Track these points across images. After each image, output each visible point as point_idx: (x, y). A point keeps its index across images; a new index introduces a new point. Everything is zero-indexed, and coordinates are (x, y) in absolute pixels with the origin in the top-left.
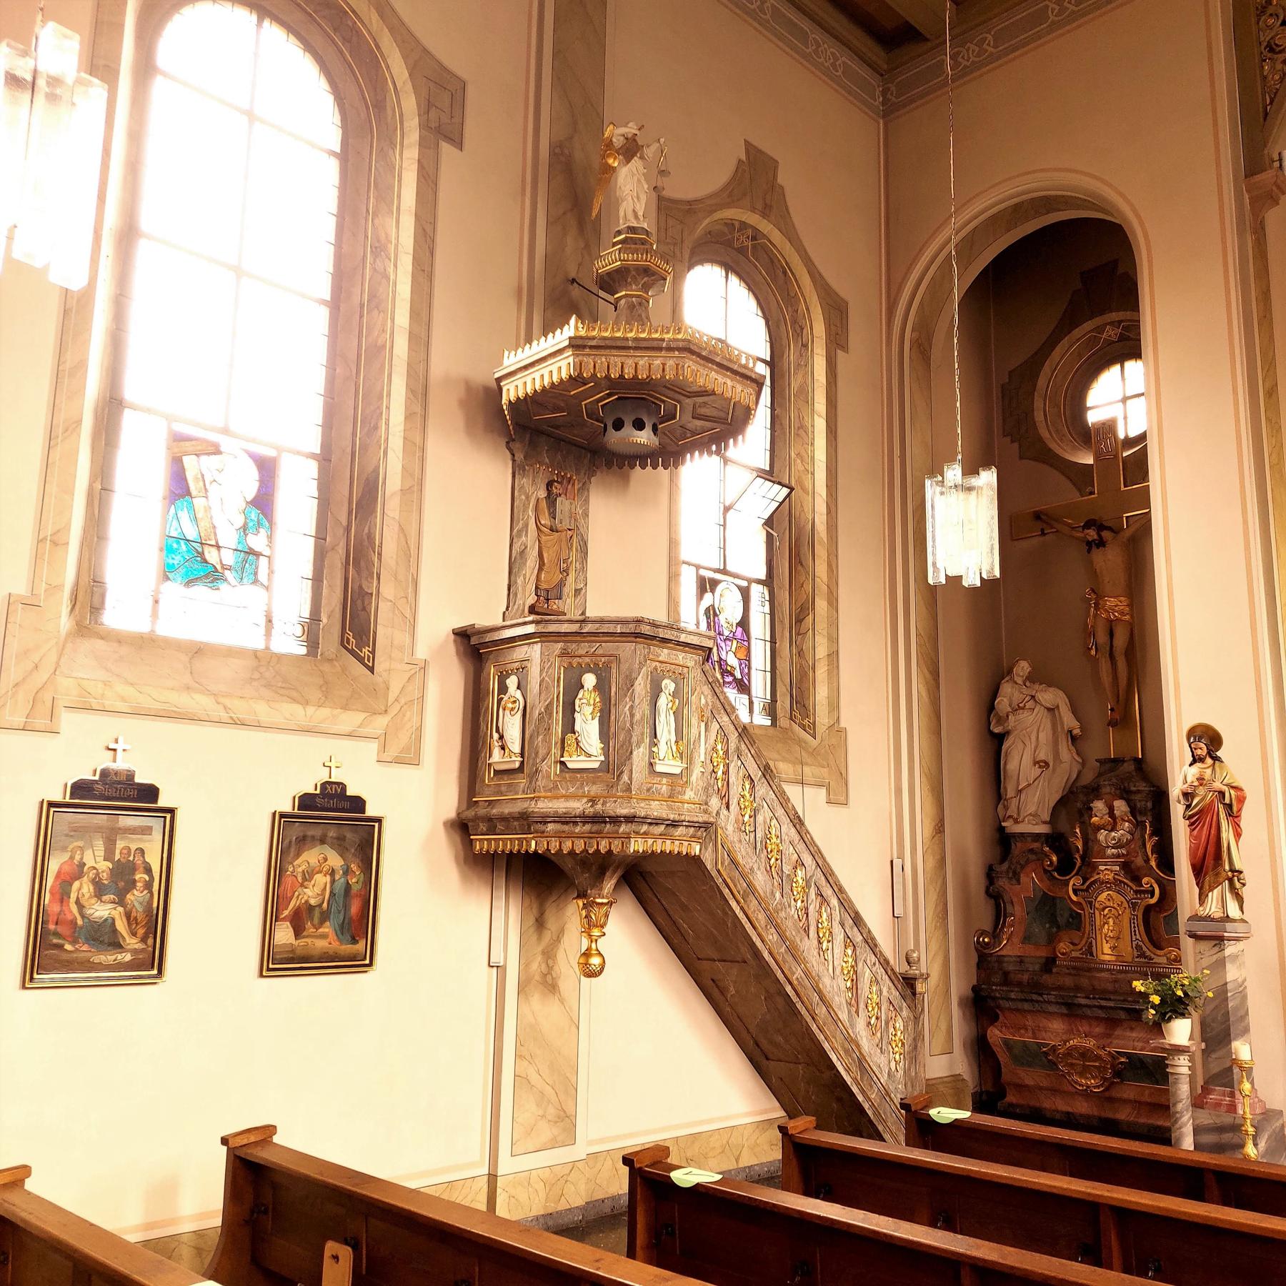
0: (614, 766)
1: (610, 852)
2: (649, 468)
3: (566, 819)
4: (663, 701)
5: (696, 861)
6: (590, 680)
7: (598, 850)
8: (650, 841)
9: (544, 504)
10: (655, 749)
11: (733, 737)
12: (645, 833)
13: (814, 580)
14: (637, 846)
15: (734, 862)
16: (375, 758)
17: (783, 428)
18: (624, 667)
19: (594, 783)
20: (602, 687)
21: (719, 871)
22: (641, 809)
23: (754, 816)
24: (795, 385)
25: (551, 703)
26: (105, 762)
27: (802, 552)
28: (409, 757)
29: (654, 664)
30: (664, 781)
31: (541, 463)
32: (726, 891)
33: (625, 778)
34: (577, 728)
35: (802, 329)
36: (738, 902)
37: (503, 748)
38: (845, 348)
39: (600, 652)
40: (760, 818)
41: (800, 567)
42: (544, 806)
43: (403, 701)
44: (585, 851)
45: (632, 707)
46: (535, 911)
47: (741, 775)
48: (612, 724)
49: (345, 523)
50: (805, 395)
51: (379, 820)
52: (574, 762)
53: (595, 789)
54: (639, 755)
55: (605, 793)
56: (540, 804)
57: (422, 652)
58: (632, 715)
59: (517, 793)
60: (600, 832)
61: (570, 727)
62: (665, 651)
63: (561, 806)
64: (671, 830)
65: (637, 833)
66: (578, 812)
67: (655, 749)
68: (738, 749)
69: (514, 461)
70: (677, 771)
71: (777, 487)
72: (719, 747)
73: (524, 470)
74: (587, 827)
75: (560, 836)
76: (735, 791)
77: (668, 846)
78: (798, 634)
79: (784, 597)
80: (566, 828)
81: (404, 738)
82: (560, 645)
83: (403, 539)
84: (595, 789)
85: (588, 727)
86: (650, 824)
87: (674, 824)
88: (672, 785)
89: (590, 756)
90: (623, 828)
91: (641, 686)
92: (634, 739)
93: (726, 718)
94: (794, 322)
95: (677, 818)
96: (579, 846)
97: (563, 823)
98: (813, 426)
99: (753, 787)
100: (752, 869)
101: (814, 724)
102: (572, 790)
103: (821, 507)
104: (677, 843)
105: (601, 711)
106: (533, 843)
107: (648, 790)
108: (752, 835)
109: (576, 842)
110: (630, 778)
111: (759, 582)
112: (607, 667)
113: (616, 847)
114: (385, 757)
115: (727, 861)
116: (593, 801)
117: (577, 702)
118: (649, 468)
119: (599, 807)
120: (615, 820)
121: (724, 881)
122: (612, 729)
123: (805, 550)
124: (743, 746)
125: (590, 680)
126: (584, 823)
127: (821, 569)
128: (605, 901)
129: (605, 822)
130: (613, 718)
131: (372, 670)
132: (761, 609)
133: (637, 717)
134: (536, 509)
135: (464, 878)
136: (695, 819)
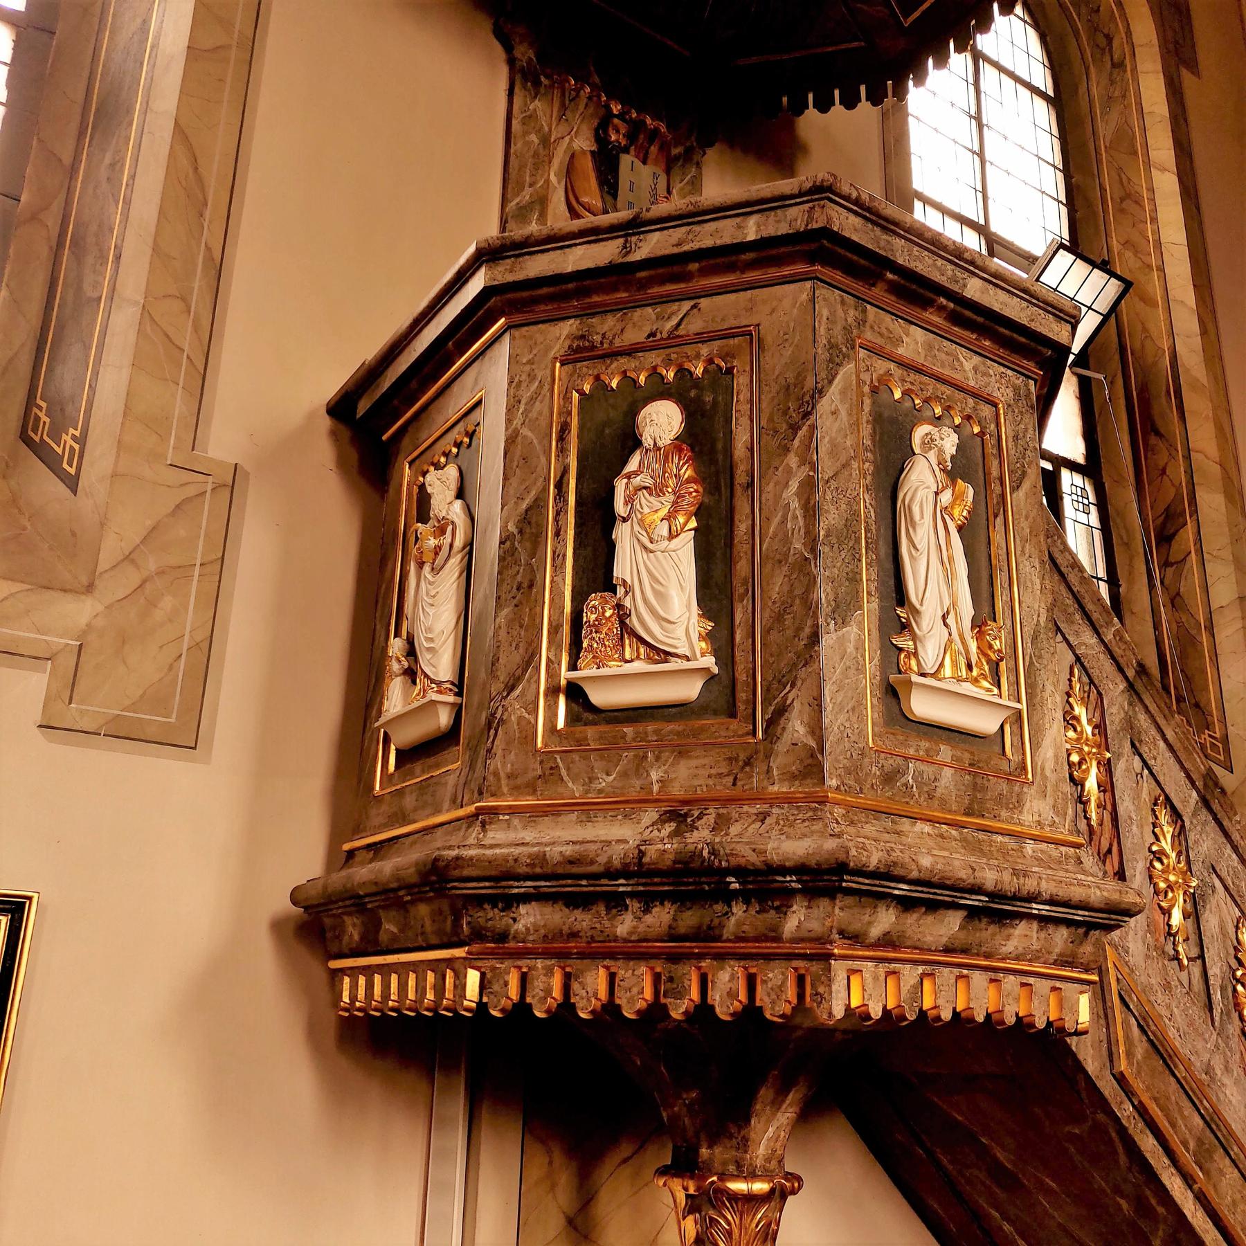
0: (751, 693)
1: (751, 1012)
2: (838, 109)
3: (576, 884)
4: (921, 479)
5: (1047, 1047)
6: (662, 421)
7: (704, 1009)
8: (910, 974)
9: (588, 164)
10: (906, 643)
11: (1115, 690)
12: (888, 942)
13: (1188, 458)
14: (857, 991)
15: (1161, 1051)
16: (38, 717)
17: (1089, 205)
18: (777, 362)
19: (682, 752)
20: (703, 439)
21: (1121, 1079)
22: (869, 845)
23: (1194, 914)
24: (1106, 130)
25: (538, 505)
27: (1156, 412)
28: (171, 724)
29: (882, 366)
30: (945, 752)
31: (582, 79)
32: (1148, 1144)
33: (796, 727)
34: (622, 569)
35: (1109, 39)
36: (1188, 1179)
37: (411, 674)
38: (1193, 66)
39: (695, 325)
40: (1210, 922)
41: (1153, 440)
42: (508, 841)
43: (152, 565)
44: (656, 1011)
45: (809, 486)
46: (564, 1197)
47: (1145, 795)
48: (741, 548)
49: (67, 159)
50: (1130, 145)
52: (618, 684)
53: (684, 776)
54: (849, 646)
55: (723, 787)
56: (496, 835)
57: (224, 443)
58: (811, 511)
59: (438, 811)
60: (707, 934)
61: (597, 571)
62: (917, 333)
63: (559, 838)
64: (986, 933)
65: (855, 938)
66: (617, 855)
67: (906, 643)
68: (1129, 723)
69: (511, 62)
70: (987, 723)
71: (1098, 276)
72: (1080, 711)
73: (536, 84)
74: (661, 917)
75: (558, 948)
76: (1135, 836)
77: (978, 997)
78: (1166, 564)
79: (1126, 497)
80: (582, 920)
81: (146, 667)
82: (568, 328)
83: (184, 162)
84: (684, 776)
85: (660, 566)
86: (907, 904)
87: (998, 909)
88: (975, 772)
89: (666, 656)
90: (798, 919)
91: (838, 420)
92: (823, 594)
93: (1089, 638)
94: (1094, 29)
95: (1009, 883)
96: (637, 990)
97: (575, 901)
98: (1151, 190)
99: (1181, 834)
100: (1209, 1070)
101: (1225, 739)
102: (605, 781)
103: (1187, 322)
104: (1011, 982)
105: (700, 512)
106: (473, 977)
107: (889, 778)
108: (1196, 970)
109: (624, 972)
110: (817, 729)
111: (1073, 466)
112: (721, 377)
113: (777, 994)
114: (73, 714)
115: (1141, 1048)
116: (679, 815)
117: (620, 486)
118: (838, 109)
119: (700, 837)
120: (767, 885)
121: (1141, 1110)
122: (742, 568)
123: (1164, 409)
124: (1142, 718)
125: (662, 421)
126: (648, 900)
127: (1202, 436)
128: (760, 1187)
129: (728, 897)
130: (742, 528)
131: (72, 483)
132: (1082, 518)
133: (830, 518)
134: (570, 171)
135: (337, 1095)
136: (1077, 893)
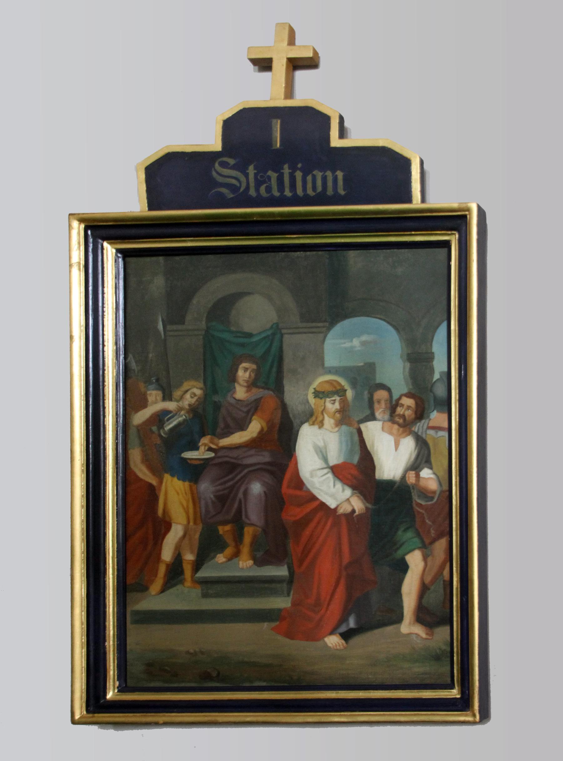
26: (264, 92)
51: (456, 221)
85: (224, 190)
